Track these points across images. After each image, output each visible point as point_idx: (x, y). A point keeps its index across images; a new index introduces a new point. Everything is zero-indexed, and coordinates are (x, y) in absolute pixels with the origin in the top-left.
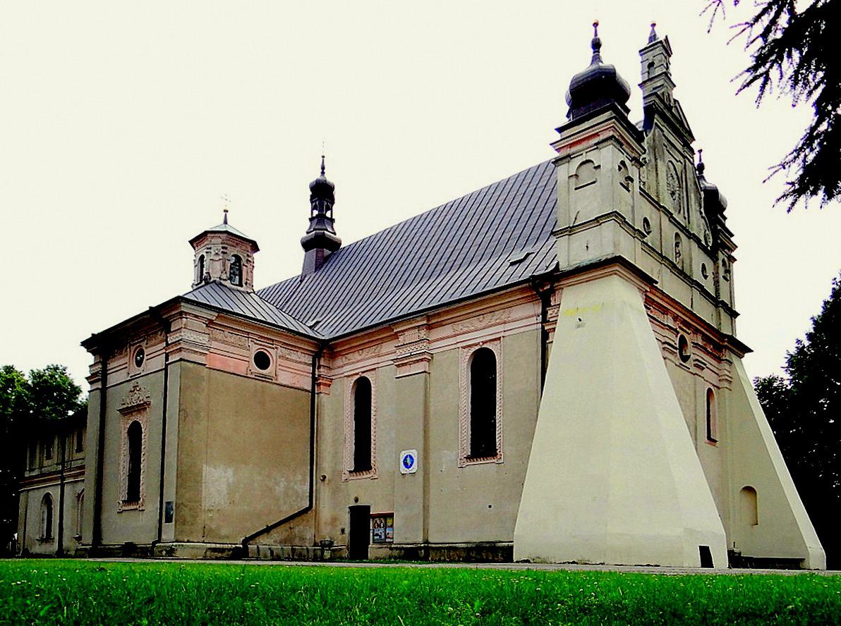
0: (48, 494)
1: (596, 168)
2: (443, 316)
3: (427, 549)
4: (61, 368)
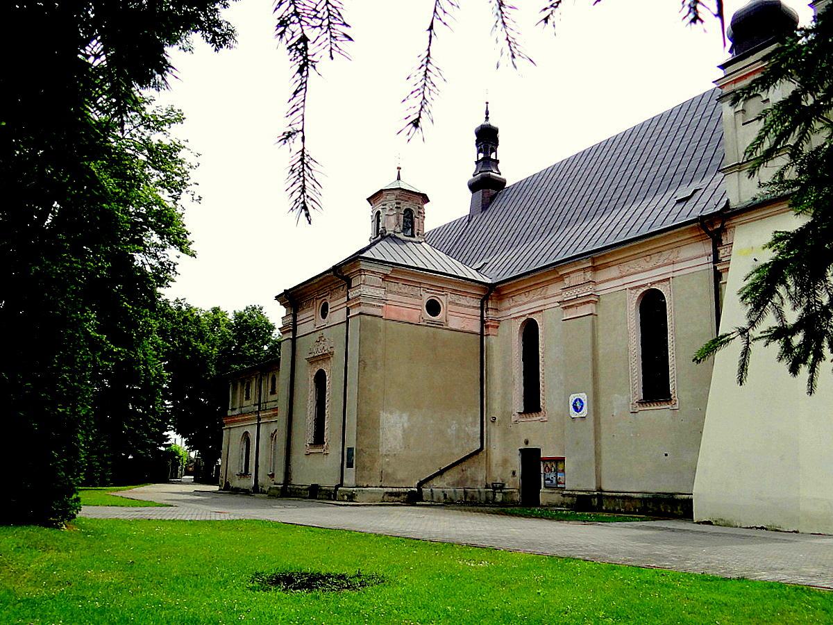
0: (247, 433)
1: (764, 101)
2: (609, 258)
3: (600, 497)
4: (258, 308)
